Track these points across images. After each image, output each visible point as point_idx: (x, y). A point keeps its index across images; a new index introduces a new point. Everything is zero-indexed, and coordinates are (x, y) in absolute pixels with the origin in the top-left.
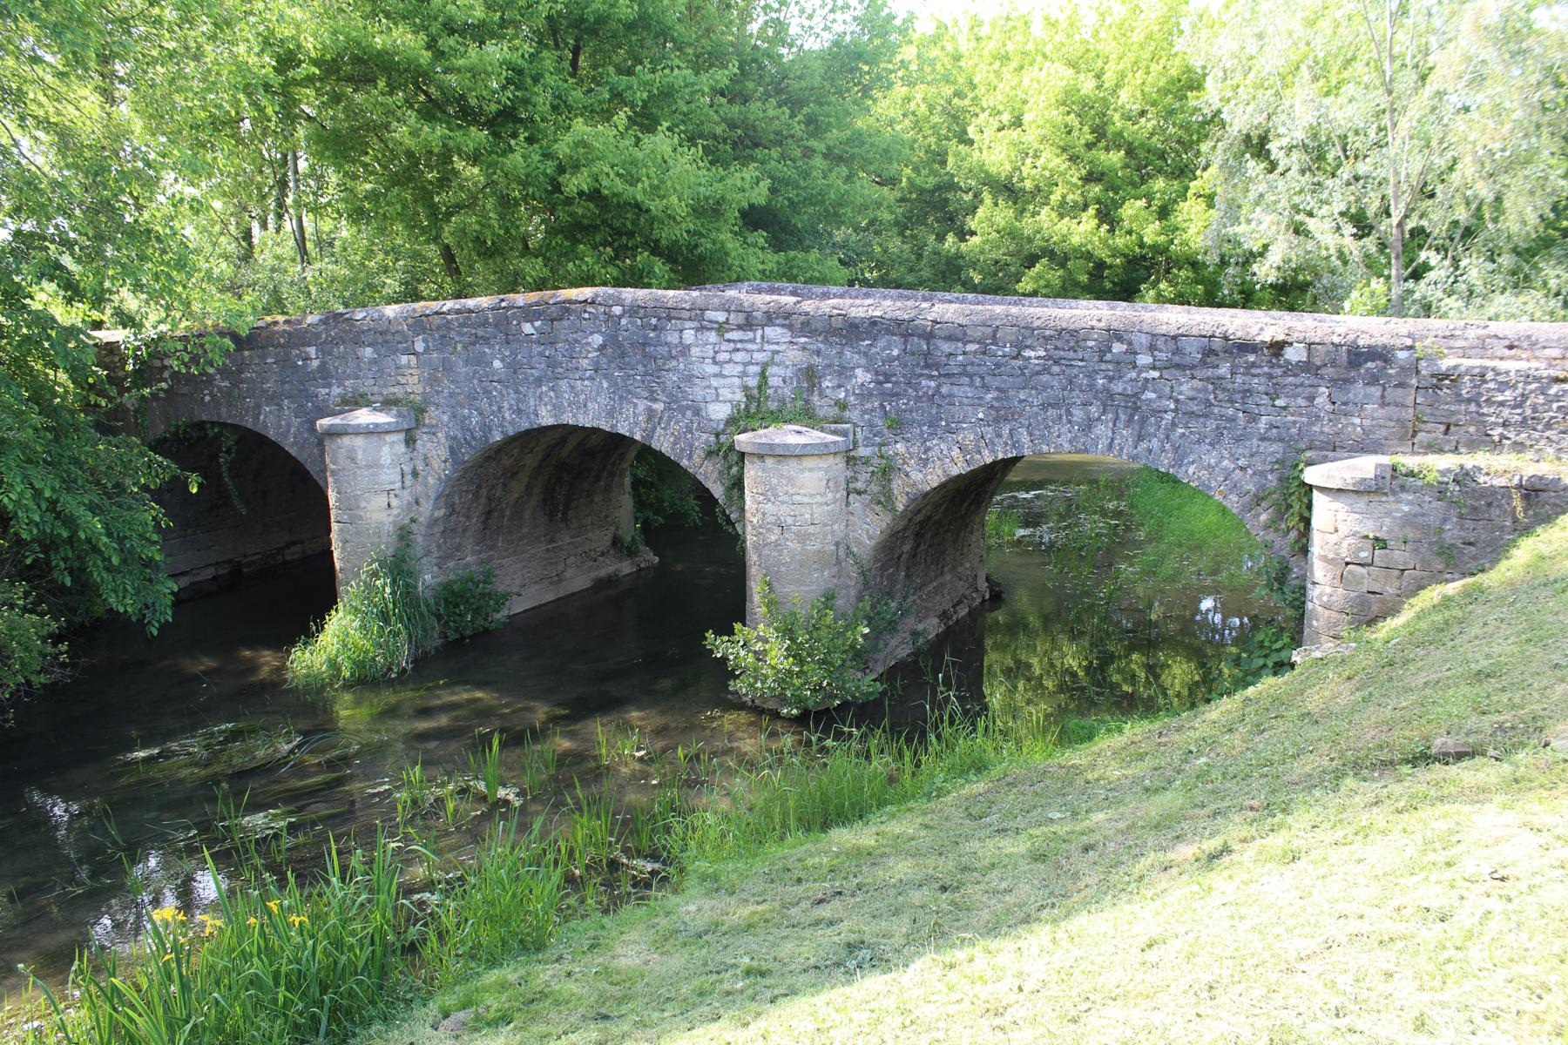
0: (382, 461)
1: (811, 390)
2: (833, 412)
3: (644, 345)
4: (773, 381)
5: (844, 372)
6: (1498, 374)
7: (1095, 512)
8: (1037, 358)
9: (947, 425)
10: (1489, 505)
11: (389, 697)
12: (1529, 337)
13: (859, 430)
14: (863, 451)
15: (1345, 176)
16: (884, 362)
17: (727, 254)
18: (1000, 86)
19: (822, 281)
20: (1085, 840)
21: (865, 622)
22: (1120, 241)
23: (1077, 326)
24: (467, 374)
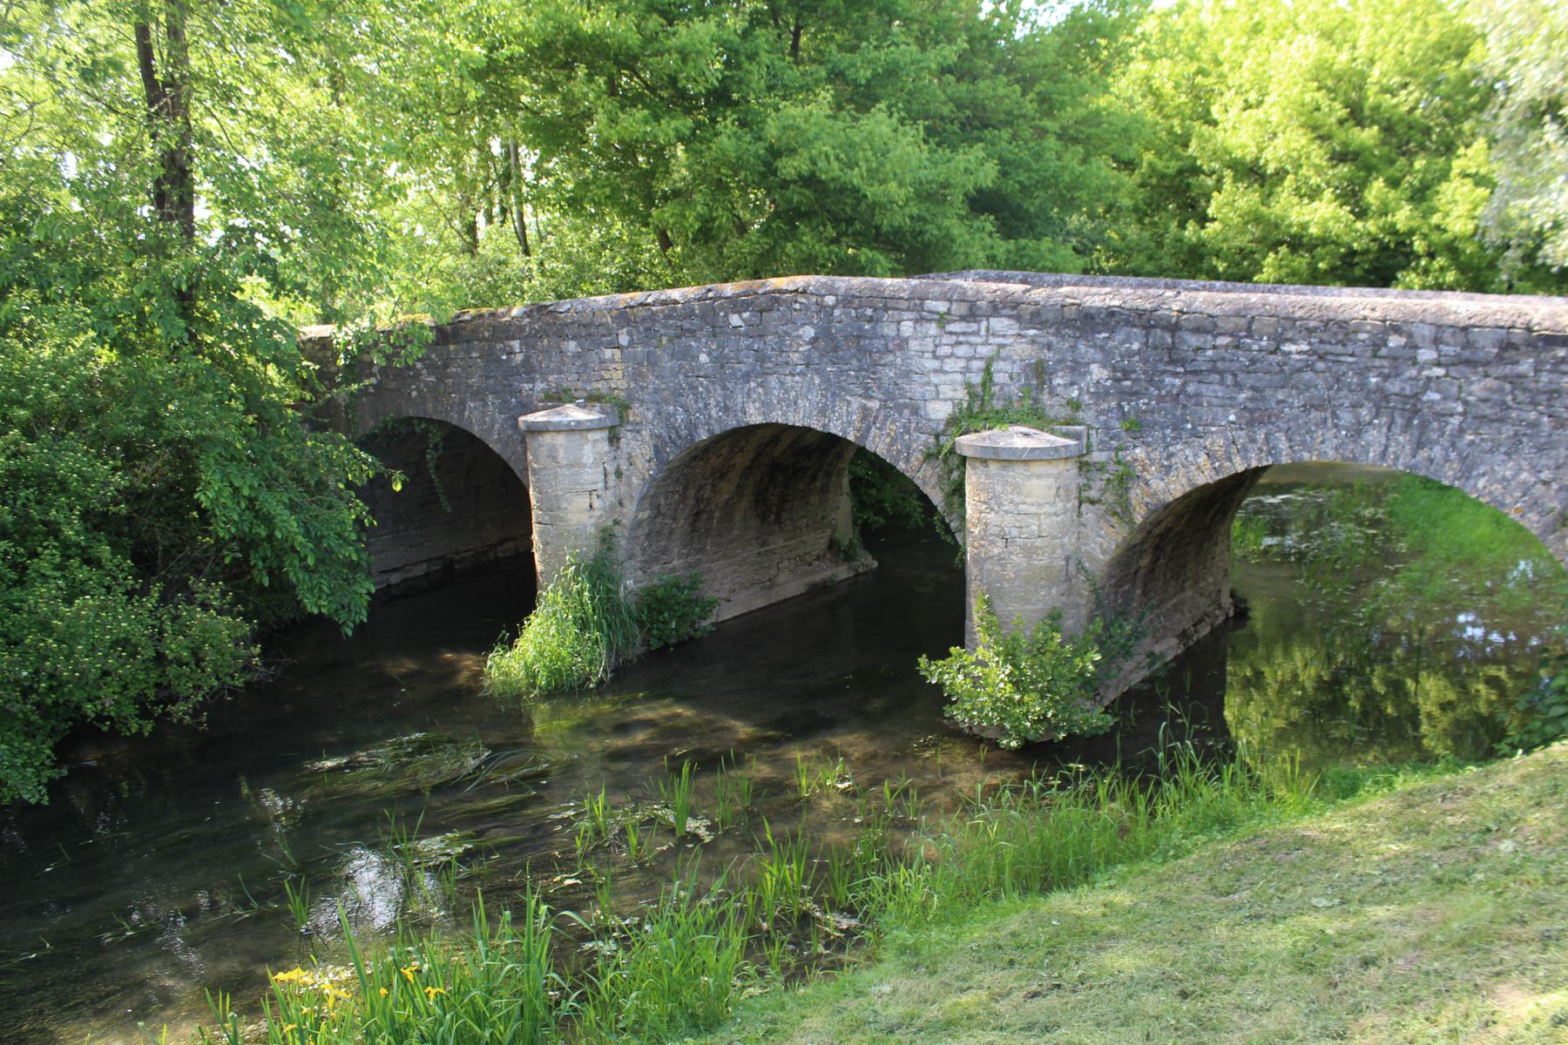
1: (1040, 388)
2: (1065, 412)
3: (859, 337)
4: (999, 378)
5: (1077, 368)
7: (1350, 520)
8: (1299, 353)
9: (1194, 428)
11: (585, 710)
13: (1093, 432)
14: (1098, 456)
16: (1122, 357)
17: (953, 241)
19: (1055, 270)
20: (1368, 948)
21: (1096, 648)
22: (1371, 226)
23: (1346, 316)
24: (672, 368)
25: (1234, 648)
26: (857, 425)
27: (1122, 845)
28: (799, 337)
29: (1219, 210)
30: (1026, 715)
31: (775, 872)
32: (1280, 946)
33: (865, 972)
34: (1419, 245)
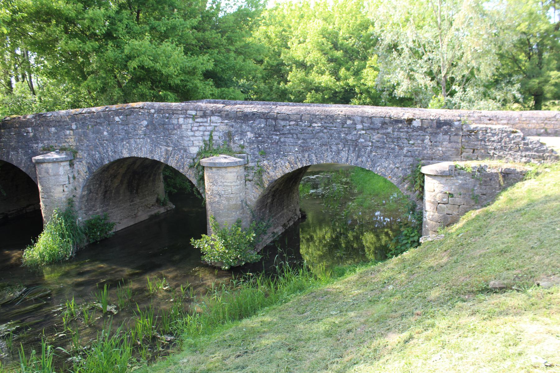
0: (60, 173)
1: (230, 141)
2: (239, 149)
3: (164, 124)
4: (215, 138)
5: (243, 134)
6: (492, 130)
7: (338, 183)
8: (318, 127)
9: (284, 153)
10: (491, 180)
12: (496, 116)
14: (251, 164)
15: (426, 59)
16: (258, 129)
17: (198, 88)
18: (299, 28)
19: (234, 99)
20: (349, 326)
21: (254, 232)
22: (342, 83)
23: (333, 114)
24: (93, 137)
25: (302, 229)
26: (164, 156)
27: (266, 300)
28: (141, 125)
29: (291, 78)
30: (230, 257)
31: (142, 322)
32: (321, 329)
33: (177, 355)
34: (357, 90)
